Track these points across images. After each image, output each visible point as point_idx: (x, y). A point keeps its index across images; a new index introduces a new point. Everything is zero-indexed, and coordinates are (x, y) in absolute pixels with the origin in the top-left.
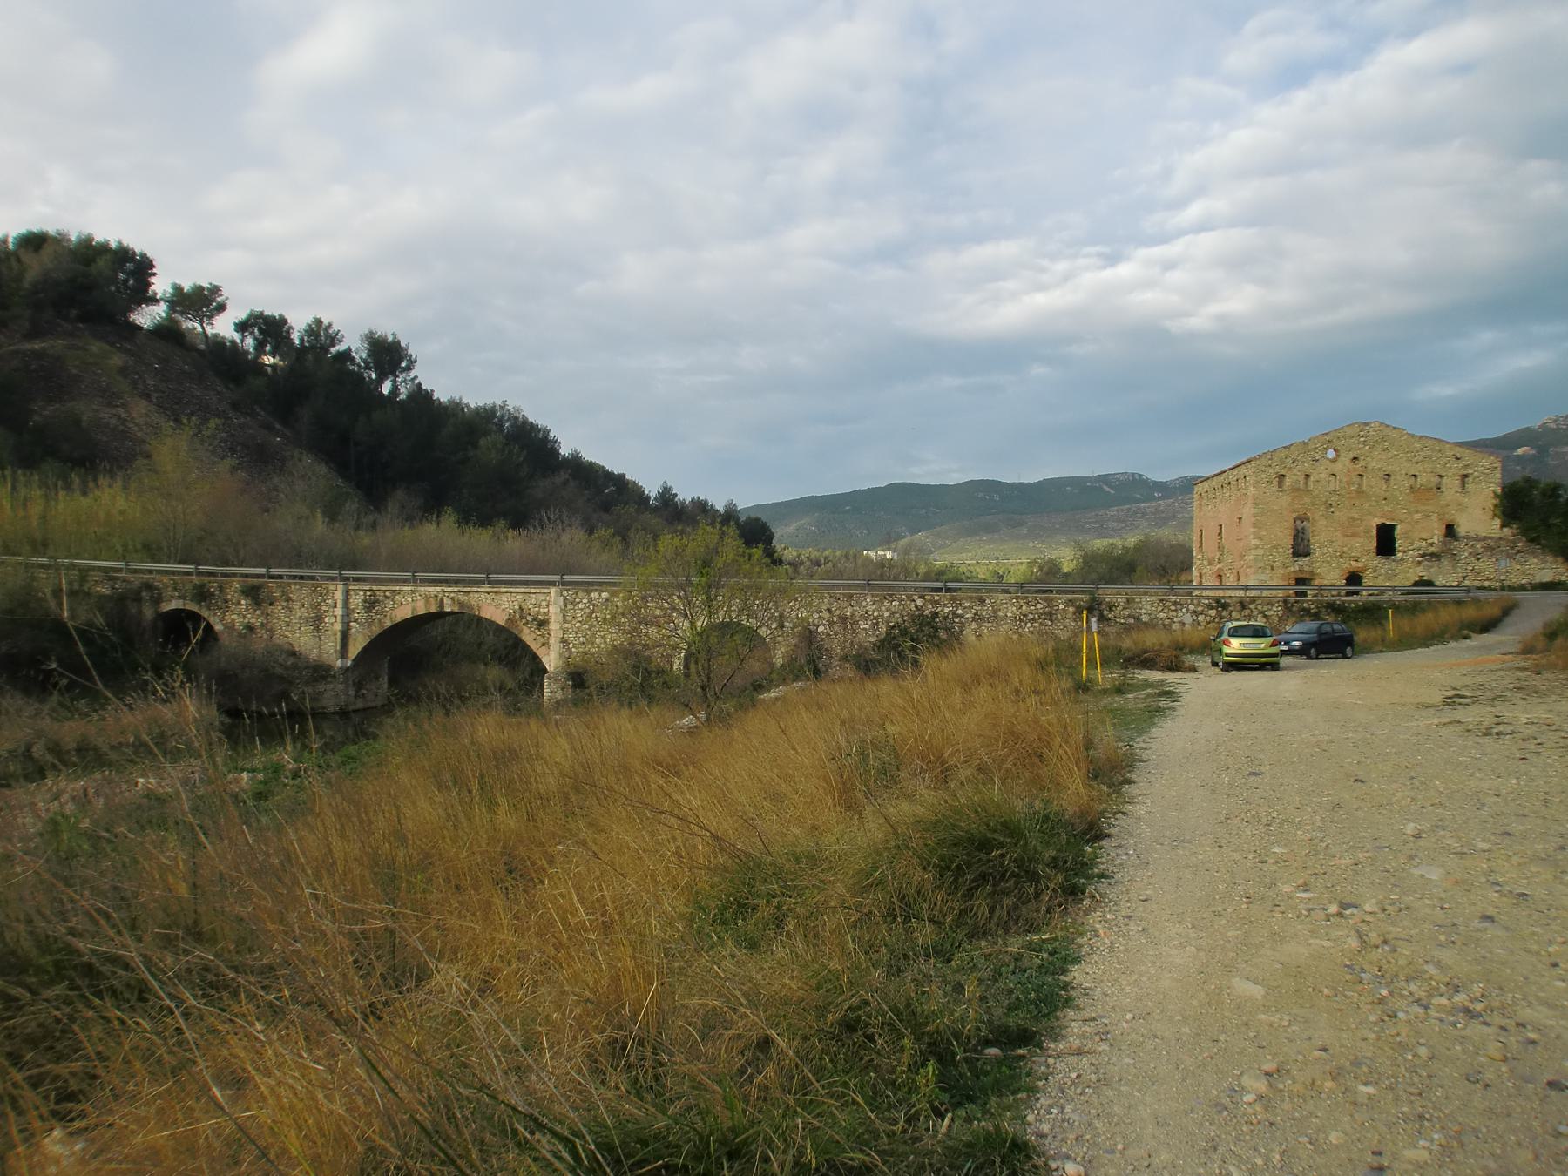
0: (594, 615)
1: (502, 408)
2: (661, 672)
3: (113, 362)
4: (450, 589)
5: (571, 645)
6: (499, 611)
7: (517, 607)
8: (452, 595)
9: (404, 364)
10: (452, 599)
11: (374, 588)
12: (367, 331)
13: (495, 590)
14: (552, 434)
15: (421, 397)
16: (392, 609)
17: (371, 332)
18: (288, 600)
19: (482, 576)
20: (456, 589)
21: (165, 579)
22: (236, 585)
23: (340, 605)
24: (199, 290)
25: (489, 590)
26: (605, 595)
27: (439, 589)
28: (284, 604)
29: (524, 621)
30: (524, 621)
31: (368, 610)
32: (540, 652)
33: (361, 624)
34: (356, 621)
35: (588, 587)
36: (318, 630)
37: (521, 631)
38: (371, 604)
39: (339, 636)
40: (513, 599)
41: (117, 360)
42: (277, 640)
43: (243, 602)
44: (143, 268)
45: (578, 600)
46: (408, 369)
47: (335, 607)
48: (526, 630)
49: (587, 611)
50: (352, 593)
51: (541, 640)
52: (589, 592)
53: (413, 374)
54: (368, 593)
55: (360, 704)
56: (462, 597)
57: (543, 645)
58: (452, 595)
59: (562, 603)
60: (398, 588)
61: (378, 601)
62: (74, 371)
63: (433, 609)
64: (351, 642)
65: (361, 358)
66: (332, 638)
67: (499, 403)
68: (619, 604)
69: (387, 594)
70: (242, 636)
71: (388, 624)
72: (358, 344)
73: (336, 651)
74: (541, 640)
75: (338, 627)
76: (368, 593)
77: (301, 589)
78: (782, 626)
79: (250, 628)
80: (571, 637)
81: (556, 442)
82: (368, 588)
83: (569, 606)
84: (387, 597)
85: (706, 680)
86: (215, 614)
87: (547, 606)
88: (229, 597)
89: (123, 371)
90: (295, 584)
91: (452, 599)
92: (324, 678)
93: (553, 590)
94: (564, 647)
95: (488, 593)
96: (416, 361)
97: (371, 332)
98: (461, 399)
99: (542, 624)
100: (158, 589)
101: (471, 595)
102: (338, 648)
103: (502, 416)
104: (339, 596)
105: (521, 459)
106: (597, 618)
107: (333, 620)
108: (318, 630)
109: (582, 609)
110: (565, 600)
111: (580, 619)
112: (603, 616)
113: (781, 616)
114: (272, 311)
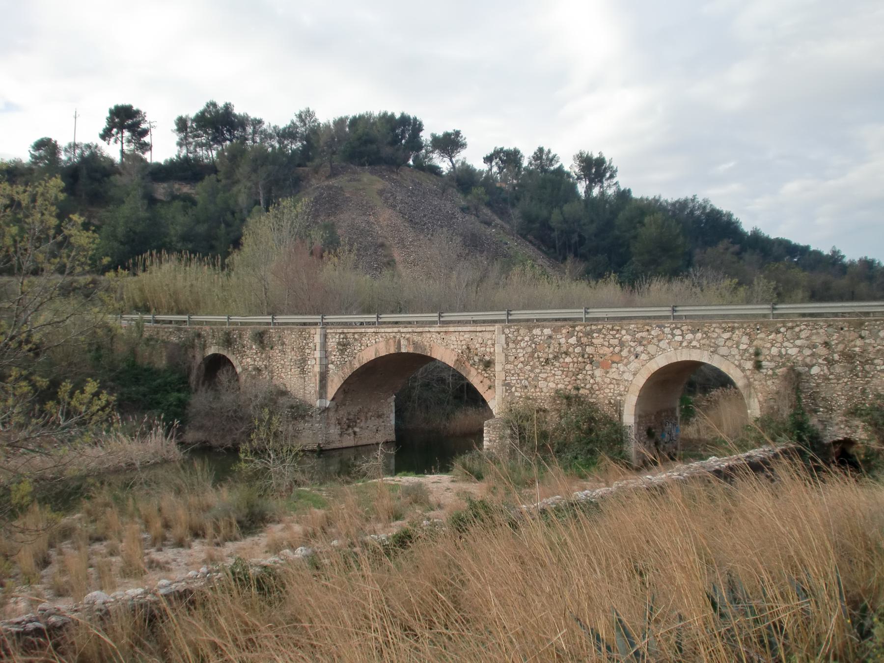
1: (693, 200)
4: (405, 330)
6: (449, 351)
11: (345, 331)
14: (734, 217)
15: (624, 196)
18: (283, 344)
20: (410, 330)
21: (207, 328)
23: (318, 348)
24: (447, 135)
25: (438, 329)
27: (396, 330)
28: (280, 348)
31: (342, 352)
34: (332, 363)
36: (303, 371)
38: (344, 346)
39: (318, 377)
42: (276, 381)
43: (254, 347)
44: (417, 127)
46: (611, 177)
48: (473, 372)
49: (529, 350)
51: (487, 382)
52: (530, 329)
53: (615, 180)
56: (416, 338)
58: (408, 336)
60: (363, 330)
66: (313, 379)
67: (690, 197)
69: (356, 336)
70: (253, 377)
71: (357, 366)
74: (487, 382)
75: (317, 369)
78: (758, 366)
79: (258, 370)
82: (340, 331)
83: (511, 345)
84: (356, 340)
87: (493, 345)
89: (381, 193)
93: (497, 327)
99: (488, 364)
104: (317, 339)
108: (303, 371)
110: (507, 338)
113: (757, 354)
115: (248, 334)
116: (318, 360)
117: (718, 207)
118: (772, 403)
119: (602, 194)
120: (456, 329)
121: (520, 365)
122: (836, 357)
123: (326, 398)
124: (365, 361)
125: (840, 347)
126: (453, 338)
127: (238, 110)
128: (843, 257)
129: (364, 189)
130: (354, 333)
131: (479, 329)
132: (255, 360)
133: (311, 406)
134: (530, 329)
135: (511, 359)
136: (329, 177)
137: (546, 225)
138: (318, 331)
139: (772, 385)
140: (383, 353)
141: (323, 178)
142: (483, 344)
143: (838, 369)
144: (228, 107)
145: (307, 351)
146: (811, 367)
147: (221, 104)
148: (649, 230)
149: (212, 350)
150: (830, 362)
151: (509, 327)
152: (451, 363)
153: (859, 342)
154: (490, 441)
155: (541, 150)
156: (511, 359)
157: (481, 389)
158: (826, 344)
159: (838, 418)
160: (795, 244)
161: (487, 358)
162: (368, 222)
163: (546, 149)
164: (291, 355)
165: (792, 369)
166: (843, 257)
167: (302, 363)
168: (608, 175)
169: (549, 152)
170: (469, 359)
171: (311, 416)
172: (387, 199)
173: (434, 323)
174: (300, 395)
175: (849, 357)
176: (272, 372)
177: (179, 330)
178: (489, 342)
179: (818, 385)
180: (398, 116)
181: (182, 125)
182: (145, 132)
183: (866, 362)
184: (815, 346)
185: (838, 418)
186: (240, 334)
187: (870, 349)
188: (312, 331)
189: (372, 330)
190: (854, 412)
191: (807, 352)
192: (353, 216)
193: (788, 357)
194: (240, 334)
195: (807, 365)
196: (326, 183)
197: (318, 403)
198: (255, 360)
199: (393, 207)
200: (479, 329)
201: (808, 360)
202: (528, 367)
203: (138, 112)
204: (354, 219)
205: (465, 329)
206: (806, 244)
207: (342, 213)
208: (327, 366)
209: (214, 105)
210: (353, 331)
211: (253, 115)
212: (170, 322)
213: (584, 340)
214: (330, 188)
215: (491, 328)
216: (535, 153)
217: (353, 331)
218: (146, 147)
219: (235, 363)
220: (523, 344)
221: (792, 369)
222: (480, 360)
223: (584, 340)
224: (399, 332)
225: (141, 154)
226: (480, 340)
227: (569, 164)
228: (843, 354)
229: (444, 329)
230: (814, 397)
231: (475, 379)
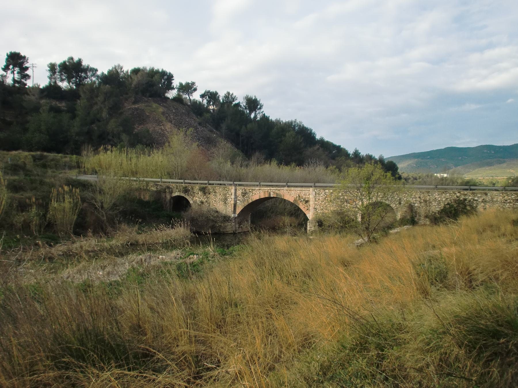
1: (295, 122)
4: (273, 189)
6: (291, 197)
7: (298, 195)
11: (246, 188)
13: (289, 189)
14: (313, 131)
15: (265, 119)
17: (247, 96)
18: (215, 192)
20: (275, 189)
21: (174, 185)
23: (233, 194)
24: (187, 84)
25: (287, 189)
27: (269, 188)
28: (214, 194)
31: (243, 196)
34: (239, 200)
36: (225, 203)
38: (244, 194)
39: (233, 205)
41: (161, 110)
42: (211, 207)
43: (200, 193)
44: (170, 77)
46: (260, 108)
48: (301, 204)
49: (324, 197)
51: (306, 208)
52: (324, 190)
53: (262, 110)
56: (277, 192)
58: (274, 191)
60: (254, 188)
63: (267, 196)
66: (231, 206)
67: (294, 120)
69: (250, 190)
70: (200, 205)
71: (250, 201)
74: (306, 208)
75: (233, 202)
78: (400, 203)
79: (202, 202)
82: (243, 188)
83: (317, 195)
84: (250, 192)
87: (309, 195)
89: (163, 113)
92: (227, 221)
93: (311, 189)
97: (247, 96)
99: (307, 202)
100: (172, 189)
104: (233, 191)
108: (225, 203)
110: (316, 193)
113: (400, 199)
115: (197, 187)
116: (233, 199)
117: (305, 126)
118: (404, 214)
119: (255, 117)
120: (294, 189)
121: (320, 202)
122: (422, 201)
123: (236, 213)
124: (254, 200)
125: (423, 198)
126: (293, 192)
127: (85, 63)
128: (360, 153)
129: (154, 111)
130: (249, 189)
131: (303, 189)
132: (200, 199)
133: (230, 217)
134: (324, 190)
135: (317, 200)
136: (134, 103)
137: (238, 134)
138: (233, 188)
139: (405, 209)
140: (262, 197)
141: (131, 103)
142: (305, 195)
143: (422, 204)
144: (80, 62)
145: (228, 195)
146: (415, 204)
147: (76, 59)
148: (289, 138)
149: (176, 194)
150: (420, 203)
151: (316, 189)
152: (292, 201)
153: (428, 197)
154: (310, 227)
155: (229, 93)
156: (317, 200)
157: (303, 210)
158: (420, 197)
159: (422, 218)
160: (327, 142)
161: (307, 199)
162: (162, 129)
163: (231, 93)
164: (219, 197)
165: (410, 205)
166: (360, 153)
167: (225, 200)
168: (259, 107)
169: (232, 94)
170: (299, 199)
171: (231, 220)
172: (167, 117)
173: (285, 186)
174: (224, 212)
175: (425, 201)
176: (209, 203)
177: (157, 185)
178: (308, 194)
179: (417, 209)
180: (160, 70)
181: (52, 68)
182: (27, 68)
183: (430, 203)
184: (416, 198)
185: (422, 218)
186: (192, 188)
187: (431, 199)
188: (230, 188)
189: (258, 188)
190: (426, 217)
191: (414, 199)
192: (154, 126)
193: (409, 201)
194: (192, 188)
195: (414, 203)
196: (133, 106)
197: (233, 215)
198: (200, 199)
199: (171, 122)
200: (303, 189)
201: (414, 202)
202: (324, 203)
203: (24, 57)
204: (154, 127)
205: (298, 189)
206: (339, 145)
207: (147, 124)
208: (236, 202)
209: (72, 59)
210: (249, 188)
211: (92, 66)
212: (197, 183)
213: (344, 194)
214: (137, 109)
215: (309, 189)
216: (226, 95)
217: (249, 188)
218: (27, 77)
219: (189, 199)
220: (321, 195)
221: (410, 205)
222: (304, 200)
223: (344, 194)
224: (270, 189)
225: (24, 81)
226: (304, 193)
227: (240, 100)
228: (424, 200)
229: (289, 189)
230: (416, 212)
231: (302, 206)
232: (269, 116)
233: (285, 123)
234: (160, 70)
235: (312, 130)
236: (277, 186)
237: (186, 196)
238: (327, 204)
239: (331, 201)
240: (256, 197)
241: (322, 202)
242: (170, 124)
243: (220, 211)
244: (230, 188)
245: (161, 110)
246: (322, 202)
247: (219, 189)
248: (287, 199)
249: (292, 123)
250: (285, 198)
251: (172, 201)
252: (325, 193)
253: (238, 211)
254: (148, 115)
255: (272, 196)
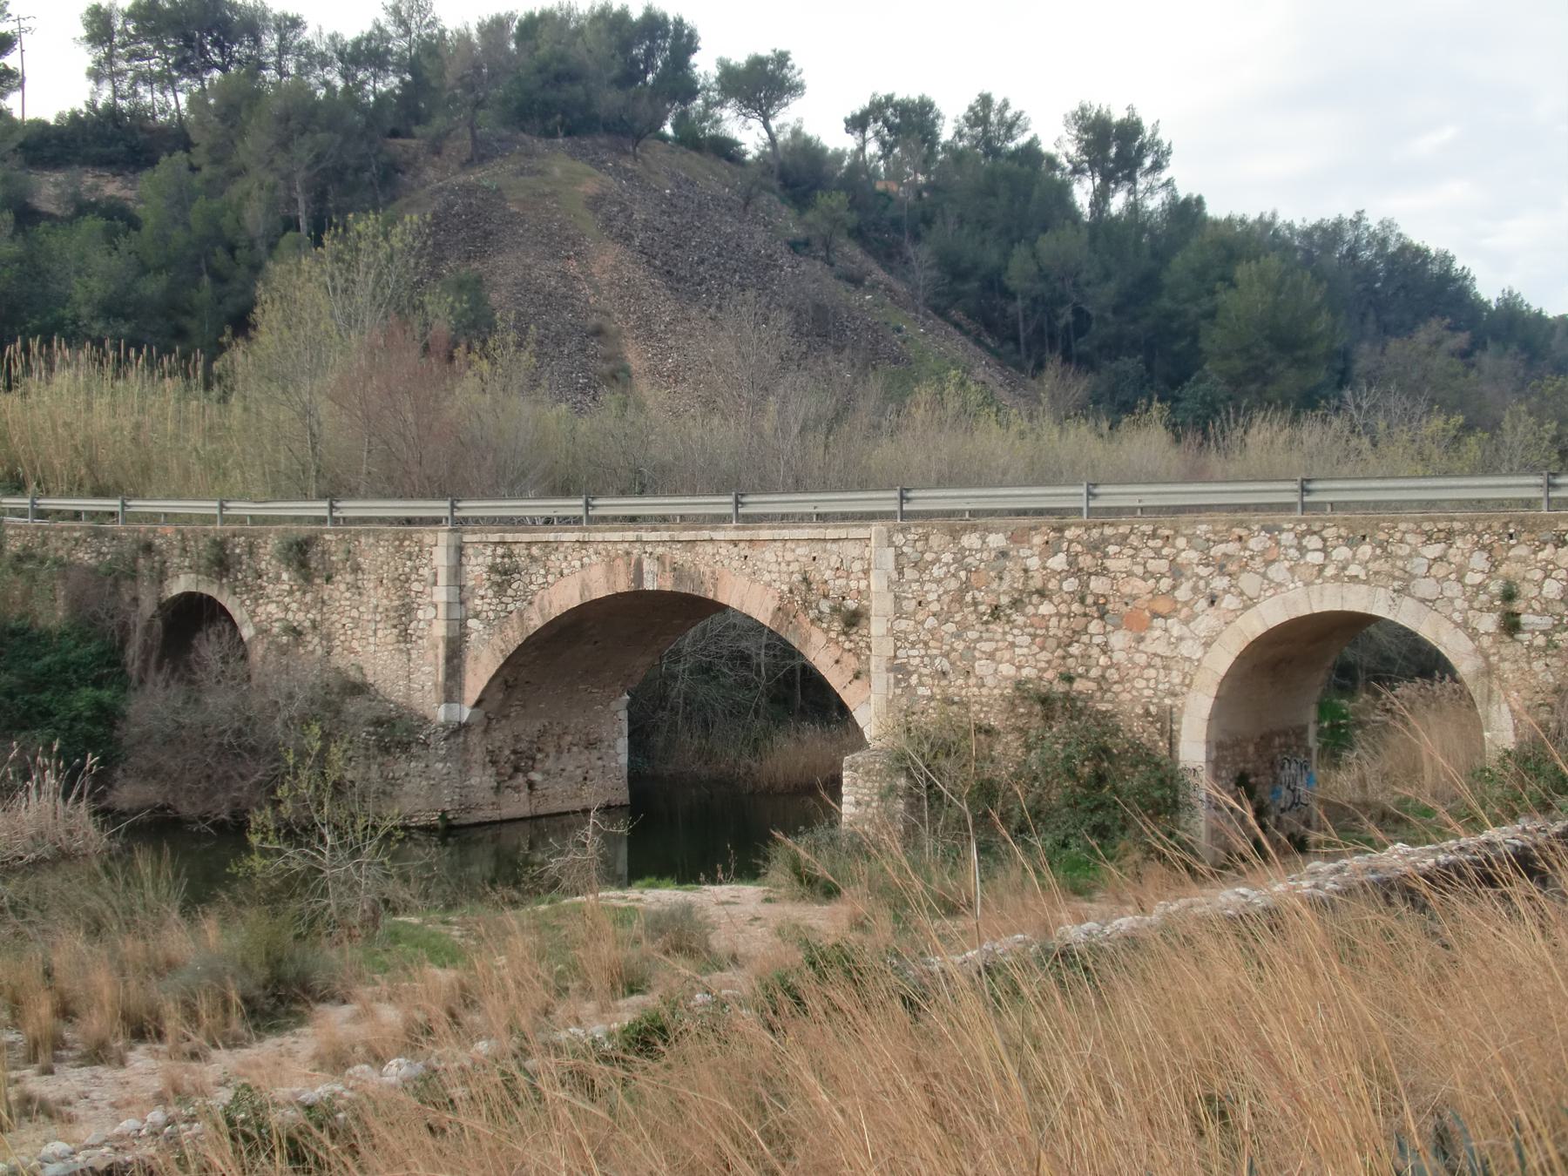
0: (968, 598)
1: (1355, 224)
2: (1143, 756)
3: (582, 189)
4: (653, 536)
5: (914, 679)
6: (758, 588)
7: (797, 577)
8: (660, 550)
9: (1148, 162)
10: (660, 559)
11: (509, 537)
12: (1076, 108)
13: (746, 535)
14: (1458, 265)
15: (1187, 213)
16: (542, 587)
17: (1083, 109)
18: (356, 569)
19: (722, 504)
20: (665, 536)
21: (169, 530)
22: (270, 545)
23: (442, 579)
24: (757, 63)
25: (733, 535)
26: (997, 540)
27: (631, 536)
28: (349, 578)
29: (812, 613)
30: (812, 613)
31: (501, 588)
32: (850, 695)
33: (488, 623)
34: (476, 616)
35: (955, 522)
36: (405, 636)
37: (807, 640)
38: (504, 575)
39: (441, 651)
40: (789, 556)
41: (591, 184)
42: (338, 660)
43: (285, 576)
44: (684, 42)
45: (929, 556)
46: (1157, 167)
47: (435, 583)
48: (818, 637)
49: (953, 584)
50: (470, 551)
51: (851, 662)
52: (955, 534)
53: (1164, 176)
54: (500, 551)
55: (516, 804)
56: (680, 556)
57: (857, 676)
58: (660, 550)
59: (891, 565)
60: (551, 537)
61: (517, 570)
62: (514, 209)
63: (623, 585)
64: (469, 665)
65: (1067, 155)
66: (430, 655)
67: (1349, 215)
68: (1034, 563)
69: (535, 551)
70: (283, 651)
71: (536, 622)
72: (1061, 131)
73: (435, 685)
74: (851, 662)
75: (440, 630)
76: (500, 551)
77: (376, 545)
78: (1511, 625)
79: (296, 632)
80: (913, 657)
81: (1465, 278)
82: (495, 538)
83: (910, 574)
84: (533, 559)
85: (100, 888)
86: (243, 602)
87: (866, 572)
88: (263, 566)
89: (595, 203)
90: (367, 533)
91: (660, 559)
92: (405, 747)
93: (875, 529)
94: (898, 682)
95: (735, 543)
96: (1169, 153)
97: (1083, 109)
98: (1274, 215)
99: (853, 619)
100: (160, 553)
101: (699, 549)
102: (441, 678)
103: (1357, 239)
104: (441, 558)
105: (1317, 299)
106: (975, 603)
107: (431, 613)
108: (405, 636)
109: (939, 581)
110: (899, 555)
111: (935, 607)
112: (990, 599)
113: (1509, 595)
114: (907, 91)
116: (442, 609)
120: (777, 534)
123: (461, 701)
124: (556, 612)
130: (529, 543)
132: (287, 609)
133: (425, 720)
134: (955, 534)
135: (909, 606)
137: (994, 284)
141: (454, 166)
142: (841, 570)
145: (416, 587)
149: (180, 585)
151: (904, 530)
152: (764, 617)
155: (986, 101)
156: (909, 606)
161: (851, 604)
162: (564, 276)
163: (997, 101)
169: (1006, 105)
170: (806, 605)
171: (426, 745)
176: (328, 637)
177: (98, 534)
180: (636, 14)
186: (251, 545)
188: (428, 539)
194: (251, 545)
196: (462, 178)
198: (287, 609)
202: (950, 627)
204: (529, 267)
208: (463, 624)
210: (526, 537)
212: (77, 515)
213: (1086, 561)
214: (469, 190)
215: (860, 533)
217: (526, 537)
219: (238, 614)
220: (937, 571)
223: (1086, 561)
224: (639, 541)
232: (1274, 215)
233: (1307, 234)
234: (636, 14)
235: (1452, 260)
236: (822, 517)
237: (226, 592)
238: (972, 635)
239: (996, 611)
240: (563, 596)
241: (943, 617)
242: (618, 248)
243: (380, 684)
244: (428, 539)
245: (591, 184)
246: (943, 617)
247: (375, 553)
248: (734, 603)
249: (1338, 225)
250: (723, 598)
251: (158, 623)
252: (959, 560)
253: (476, 679)
254: (513, 215)
255: (650, 585)
